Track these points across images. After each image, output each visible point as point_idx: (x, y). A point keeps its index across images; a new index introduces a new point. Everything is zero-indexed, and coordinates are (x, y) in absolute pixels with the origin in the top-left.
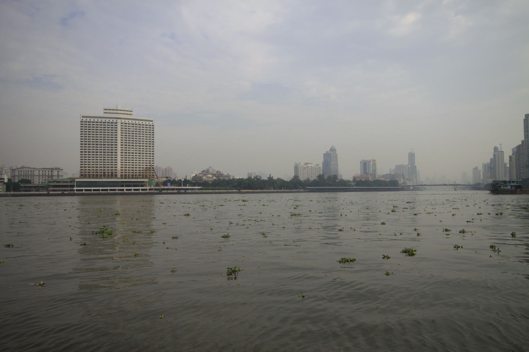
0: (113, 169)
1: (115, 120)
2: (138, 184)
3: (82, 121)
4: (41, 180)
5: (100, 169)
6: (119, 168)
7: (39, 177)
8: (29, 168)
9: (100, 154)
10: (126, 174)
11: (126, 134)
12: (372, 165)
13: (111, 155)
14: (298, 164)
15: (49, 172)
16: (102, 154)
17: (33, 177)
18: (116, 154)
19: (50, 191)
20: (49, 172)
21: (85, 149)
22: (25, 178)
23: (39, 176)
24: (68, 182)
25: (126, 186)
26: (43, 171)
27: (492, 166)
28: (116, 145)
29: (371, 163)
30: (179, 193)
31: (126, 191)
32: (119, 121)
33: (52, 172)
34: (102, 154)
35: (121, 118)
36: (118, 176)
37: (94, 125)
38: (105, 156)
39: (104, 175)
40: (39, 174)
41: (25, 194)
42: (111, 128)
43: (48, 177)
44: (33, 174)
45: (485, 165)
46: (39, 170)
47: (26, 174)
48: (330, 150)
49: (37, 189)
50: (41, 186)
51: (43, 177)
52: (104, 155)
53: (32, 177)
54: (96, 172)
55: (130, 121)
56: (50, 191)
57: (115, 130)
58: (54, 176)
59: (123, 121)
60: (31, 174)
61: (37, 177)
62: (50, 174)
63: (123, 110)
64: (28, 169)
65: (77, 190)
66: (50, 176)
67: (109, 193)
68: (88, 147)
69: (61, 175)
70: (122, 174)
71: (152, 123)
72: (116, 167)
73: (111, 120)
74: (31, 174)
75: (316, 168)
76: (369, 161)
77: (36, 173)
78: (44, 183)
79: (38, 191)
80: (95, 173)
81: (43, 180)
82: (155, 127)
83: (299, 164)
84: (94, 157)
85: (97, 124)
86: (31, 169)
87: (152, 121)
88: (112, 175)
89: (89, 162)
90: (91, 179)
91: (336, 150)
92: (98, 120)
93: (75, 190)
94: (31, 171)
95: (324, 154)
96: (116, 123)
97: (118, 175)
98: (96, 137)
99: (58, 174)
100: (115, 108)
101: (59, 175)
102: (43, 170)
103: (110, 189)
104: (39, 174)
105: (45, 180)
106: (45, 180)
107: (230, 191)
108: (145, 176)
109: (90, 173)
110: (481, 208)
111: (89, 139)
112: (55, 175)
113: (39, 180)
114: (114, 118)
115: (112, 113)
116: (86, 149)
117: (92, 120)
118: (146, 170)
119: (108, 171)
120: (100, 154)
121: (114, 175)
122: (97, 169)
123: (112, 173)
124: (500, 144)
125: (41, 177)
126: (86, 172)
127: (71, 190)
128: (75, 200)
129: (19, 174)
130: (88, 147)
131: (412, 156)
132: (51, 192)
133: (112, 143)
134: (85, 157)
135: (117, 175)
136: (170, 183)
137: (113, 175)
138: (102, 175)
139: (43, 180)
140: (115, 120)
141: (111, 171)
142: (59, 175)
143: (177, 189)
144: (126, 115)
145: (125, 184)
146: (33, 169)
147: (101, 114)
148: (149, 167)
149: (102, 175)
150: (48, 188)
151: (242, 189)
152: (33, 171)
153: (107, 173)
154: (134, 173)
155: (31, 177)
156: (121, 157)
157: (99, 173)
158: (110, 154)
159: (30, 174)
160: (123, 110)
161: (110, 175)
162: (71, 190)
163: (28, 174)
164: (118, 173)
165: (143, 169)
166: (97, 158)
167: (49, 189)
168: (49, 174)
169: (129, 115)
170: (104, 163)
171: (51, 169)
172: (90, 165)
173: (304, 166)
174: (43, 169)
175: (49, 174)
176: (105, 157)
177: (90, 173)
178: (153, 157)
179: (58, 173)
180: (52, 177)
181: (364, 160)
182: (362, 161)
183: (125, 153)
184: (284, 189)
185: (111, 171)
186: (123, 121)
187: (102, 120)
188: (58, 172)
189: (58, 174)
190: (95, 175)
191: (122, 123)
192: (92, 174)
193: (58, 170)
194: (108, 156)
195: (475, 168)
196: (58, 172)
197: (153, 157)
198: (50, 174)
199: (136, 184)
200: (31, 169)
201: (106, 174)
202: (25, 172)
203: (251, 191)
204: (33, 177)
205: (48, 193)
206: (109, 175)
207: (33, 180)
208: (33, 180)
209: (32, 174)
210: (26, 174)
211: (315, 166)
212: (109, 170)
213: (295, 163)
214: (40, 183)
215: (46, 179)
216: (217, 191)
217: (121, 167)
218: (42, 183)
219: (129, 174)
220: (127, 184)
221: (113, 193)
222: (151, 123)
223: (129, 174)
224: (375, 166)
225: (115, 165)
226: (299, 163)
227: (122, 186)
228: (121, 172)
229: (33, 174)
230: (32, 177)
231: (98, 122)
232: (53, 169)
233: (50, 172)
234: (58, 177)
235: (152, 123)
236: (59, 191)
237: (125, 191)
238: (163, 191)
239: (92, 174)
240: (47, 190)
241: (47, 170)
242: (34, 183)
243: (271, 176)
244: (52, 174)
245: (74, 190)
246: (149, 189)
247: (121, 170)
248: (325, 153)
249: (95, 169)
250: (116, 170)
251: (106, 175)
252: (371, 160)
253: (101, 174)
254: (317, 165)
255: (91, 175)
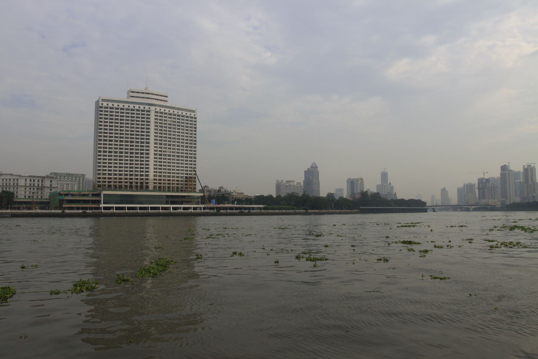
0: (144, 177)
1: (147, 108)
2: (178, 200)
3: (102, 106)
4: (28, 193)
5: (125, 177)
6: (151, 177)
7: (25, 189)
8: (12, 175)
9: (126, 155)
10: (161, 185)
11: (161, 128)
12: (360, 184)
13: (141, 157)
14: (281, 182)
15: (39, 181)
16: (128, 155)
17: (17, 188)
18: (147, 156)
19: (65, 208)
20: (39, 181)
21: (104, 148)
22: (8, 189)
23: (25, 186)
24: (87, 195)
25: (172, 203)
26: (30, 180)
27: (480, 187)
28: (148, 143)
29: (359, 182)
30: (241, 214)
31: (173, 210)
32: (153, 108)
33: (42, 181)
34: (128, 155)
35: (155, 105)
36: (150, 189)
37: (118, 112)
38: (132, 159)
39: (131, 187)
40: (26, 184)
41: (29, 213)
42: (110, 126)
43: (38, 189)
44: (17, 184)
45: (466, 185)
46: (26, 178)
47: (6, 184)
48: (311, 167)
49: (30, 206)
50: (36, 202)
51: (30, 189)
52: (131, 157)
53: (15, 189)
54: (120, 182)
55: (167, 110)
56: (65, 208)
57: (147, 122)
58: (45, 188)
59: (158, 109)
60: (14, 184)
61: (23, 189)
62: (40, 185)
63: (160, 95)
64: (9, 177)
65: (105, 208)
66: (40, 187)
67: (149, 213)
68: (109, 145)
69: (55, 186)
70: (155, 185)
71: (195, 115)
72: (147, 176)
73: (142, 107)
74: (14, 184)
75: (298, 186)
76: (357, 180)
77: (22, 182)
78: (31, 197)
79: (30, 209)
80: (117, 184)
81: (30, 193)
82: (197, 120)
83: (281, 182)
84: (116, 160)
85: (122, 111)
86: (14, 177)
87: (194, 111)
88: (141, 187)
89: (109, 167)
90: (143, 192)
91: (317, 167)
92: (124, 106)
93: (101, 207)
94: (14, 180)
95: (305, 171)
96: (149, 111)
97: (150, 186)
98: (121, 130)
99: (51, 186)
100: (142, 89)
101: (53, 186)
102: (31, 178)
103: (139, 207)
104: (26, 184)
105: (33, 193)
106: (33, 193)
107: (297, 211)
108: (163, 188)
109: (111, 184)
110: (432, 229)
111: (110, 133)
112: (47, 186)
113: (25, 193)
114: (146, 104)
115: (141, 97)
116: (106, 148)
117: (116, 105)
118: (186, 181)
119: (137, 181)
120: (126, 155)
121: (144, 186)
122: (121, 177)
123: (141, 183)
124: (508, 162)
125: (28, 189)
126: (105, 182)
127: (95, 208)
128: (85, 223)
129: (3, 184)
130: (109, 145)
131: (384, 175)
132: (67, 211)
133: (142, 141)
134: (104, 159)
135: (148, 186)
136: (215, 200)
137: (143, 186)
138: (128, 186)
139: (30, 193)
140: (147, 108)
141: (141, 181)
142: (53, 186)
143: (237, 209)
144: (159, 101)
145: (170, 200)
146: (17, 177)
147: (124, 97)
148: (190, 176)
149: (128, 186)
150: (63, 204)
151: (310, 209)
152: (17, 180)
153: (135, 184)
154: (188, 185)
155: (14, 188)
156: (155, 161)
157: (123, 183)
158: (139, 155)
159: (12, 184)
160: (160, 95)
161: (139, 186)
162: (95, 208)
163: (10, 184)
164: (150, 184)
165: (182, 179)
166: (121, 162)
167: (64, 206)
168: (38, 185)
169: (163, 102)
170: (131, 169)
171: (42, 178)
172: (111, 170)
173: (298, 185)
174: (30, 176)
175: (38, 185)
176: (122, 164)
177: (111, 184)
178: (195, 163)
179: (51, 183)
180: (42, 189)
181: (350, 178)
182: (348, 179)
183: (159, 155)
184: (345, 209)
185: (141, 181)
186: (158, 109)
187: (129, 106)
188: (51, 181)
189: (51, 186)
190: (118, 186)
191: (156, 112)
192: (124, 185)
193: (51, 179)
194: (137, 159)
195: (443, 189)
196: (51, 181)
197: (195, 163)
198: (40, 185)
199: (175, 200)
200: (14, 177)
201: (134, 184)
202: (5, 180)
203: (317, 211)
204: (17, 188)
205: (63, 212)
206: (137, 187)
207: (17, 193)
208: (17, 193)
209: (16, 184)
210: (6, 184)
211: (285, 184)
212: (137, 179)
213: (277, 181)
214: (27, 197)
215: (35, 192)
216: (270, 211)
217: (155, 176)
218: (29, 197)
219: (173, 185)
220: (172, 200)
221: (155, 213)
222: (192, 115)
223: (173, 185)
224: (363, 185)
225: (146, 172)
226: (281, 180)
227: (167, 203)
228: (154, 183)
229: (17, 184)
230: (15, 189)
231: (123, 109)
232: (44, 177)
233: (40, 181)
234: (51, 190)
235: (195, 115)
236: (78, 208)
237: (172, 210)
238: (222, 211)
239: (113, 185)
240: (60, 208)
241: (28, 178)
242: (19, 197)
243: (306, 193)
244: (42, 185)
245: (99, 208)
246: (203, 207)
247: (155, 180)
248: (307, 170)
249: (118, 177)
250: (147, 179)
251: (134, 186)
252: (359, 178)
253: (127, 184)
254: (298, 183)
255: (112, 186)
